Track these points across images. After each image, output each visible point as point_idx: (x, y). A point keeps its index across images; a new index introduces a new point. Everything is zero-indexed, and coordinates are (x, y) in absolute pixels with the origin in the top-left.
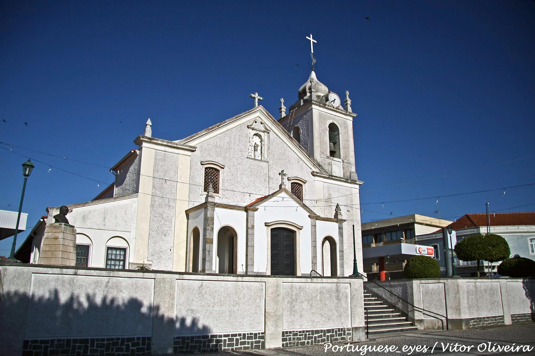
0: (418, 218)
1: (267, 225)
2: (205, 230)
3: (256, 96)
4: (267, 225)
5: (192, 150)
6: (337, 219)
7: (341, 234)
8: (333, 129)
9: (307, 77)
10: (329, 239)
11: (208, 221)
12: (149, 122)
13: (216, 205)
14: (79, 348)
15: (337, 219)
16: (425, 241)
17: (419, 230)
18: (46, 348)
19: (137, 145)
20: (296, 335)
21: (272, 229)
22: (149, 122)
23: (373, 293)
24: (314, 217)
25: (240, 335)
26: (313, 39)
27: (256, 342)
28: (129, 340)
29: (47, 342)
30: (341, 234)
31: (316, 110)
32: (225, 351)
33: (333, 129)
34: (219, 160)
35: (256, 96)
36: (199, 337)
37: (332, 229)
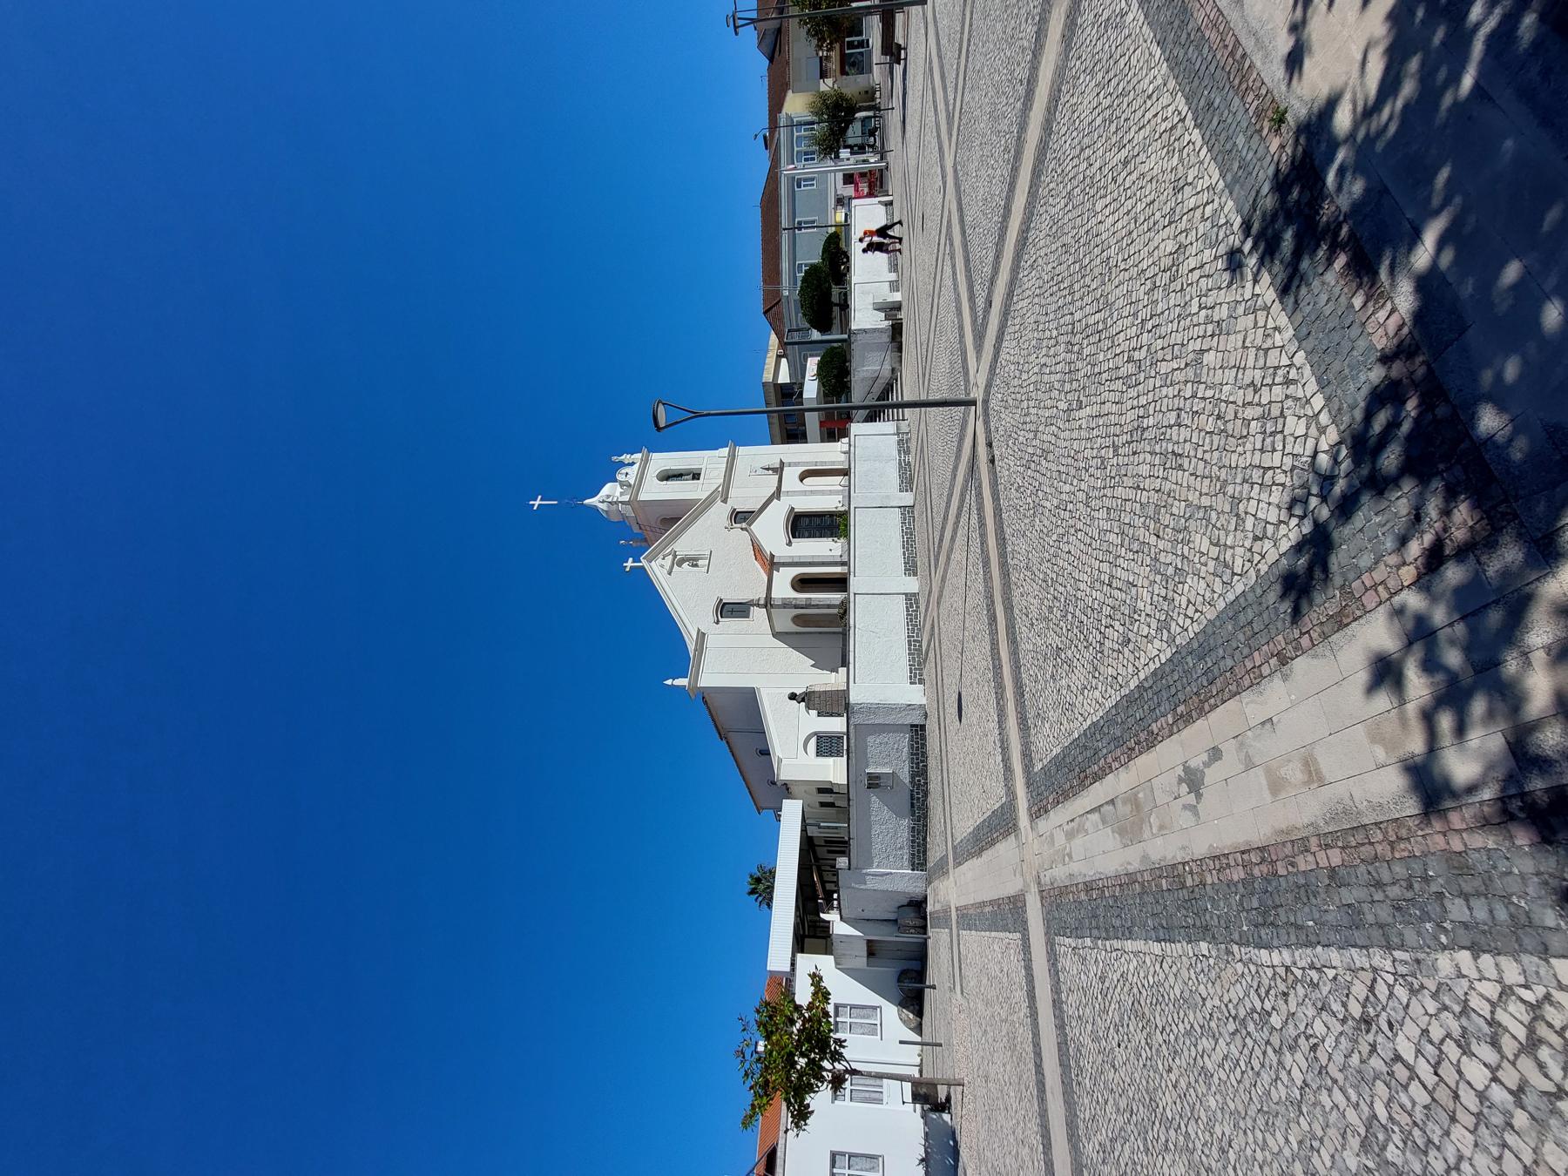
0: (768, 376)
1: (718, 622)
2: (796, 607)
3: (630, 564)
4: (790, 544)
5: (701, 636)
6: (779, 470)
7: (797, 464)
8: (668, 476)
9: (594, 509)
10: (802, 477)
11: (786, 604)
12: (669, 682)
13: (894, 434)
14: (915, 645)
15: (779, 470)
16: (798, 371)
17: (784, 377)
18: (916, 669)
19: (993, 304)
20: (902, 481)
21: (793, 537)
22: (669, 682)
23: (1441, 411)
24: (777, 494)
25: (902, 527)
26: (536, 500)
27: (909, 513)
28: (908, 611)
29: (911, 669)
30: (797, 464)
31: (643, 497)
32: (849, 150)
33: (668, 476)
34: (713, 603)
35: (630, 564)
36: (904, 558)
37: (790, 475)
